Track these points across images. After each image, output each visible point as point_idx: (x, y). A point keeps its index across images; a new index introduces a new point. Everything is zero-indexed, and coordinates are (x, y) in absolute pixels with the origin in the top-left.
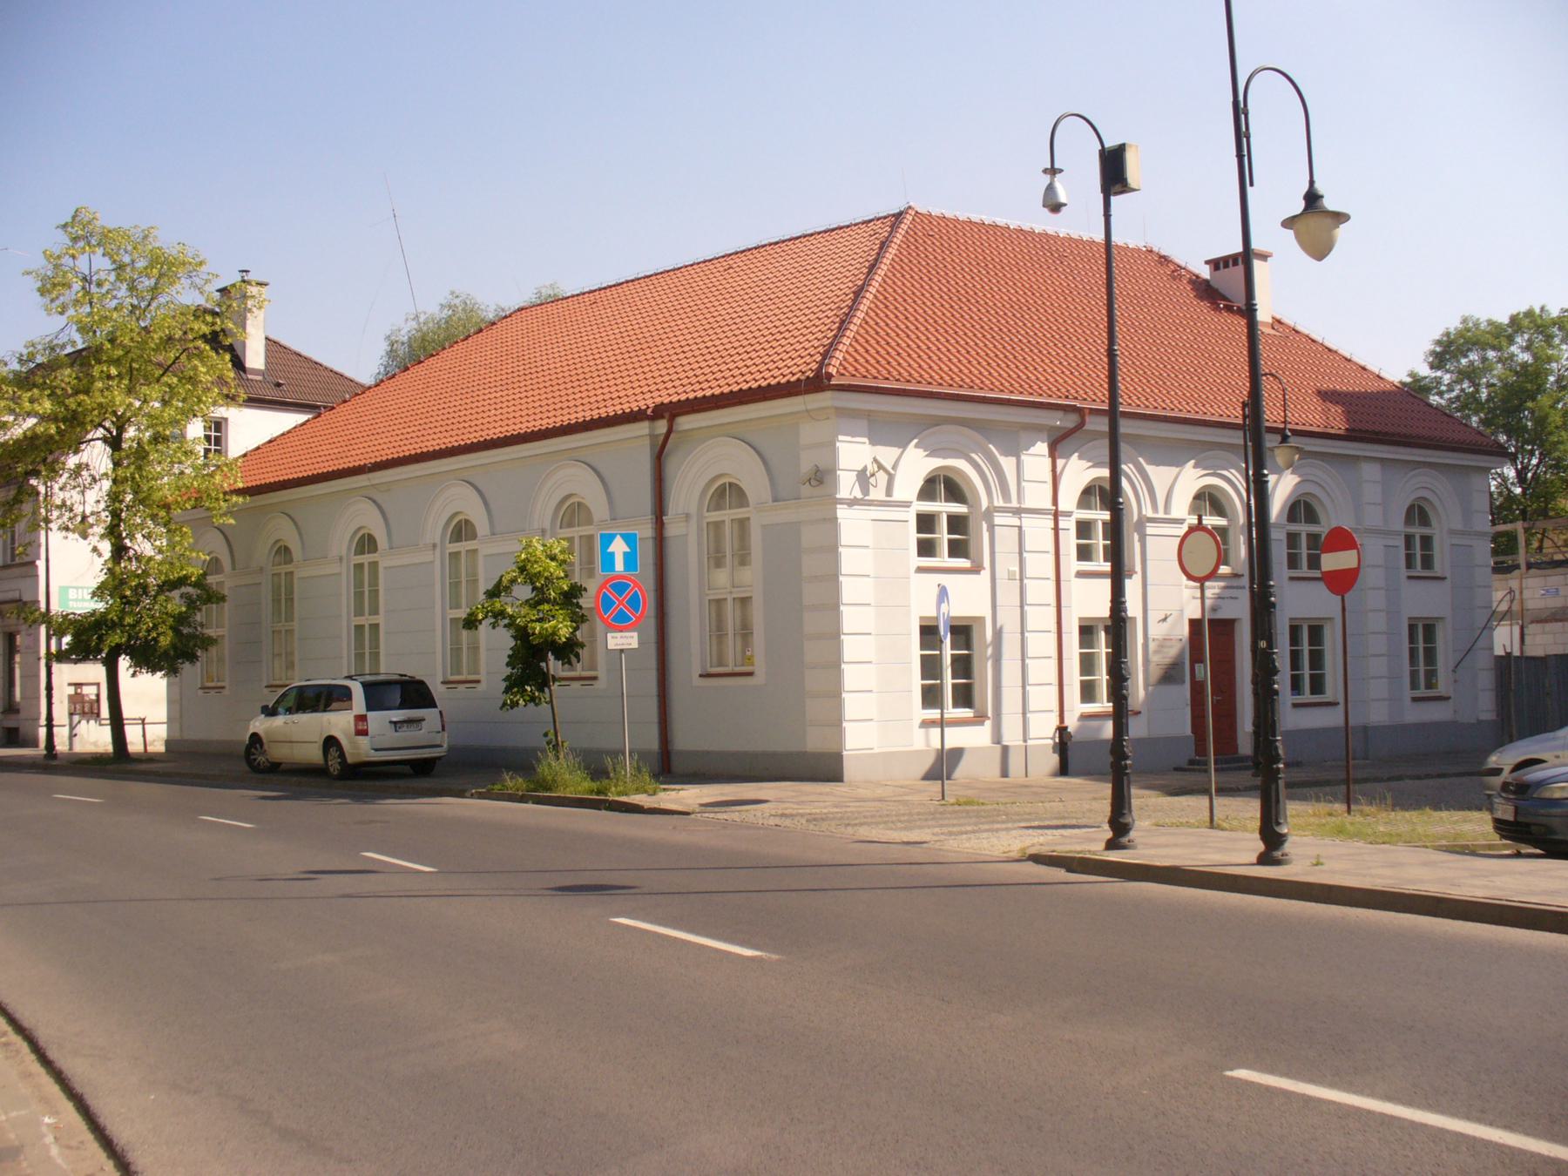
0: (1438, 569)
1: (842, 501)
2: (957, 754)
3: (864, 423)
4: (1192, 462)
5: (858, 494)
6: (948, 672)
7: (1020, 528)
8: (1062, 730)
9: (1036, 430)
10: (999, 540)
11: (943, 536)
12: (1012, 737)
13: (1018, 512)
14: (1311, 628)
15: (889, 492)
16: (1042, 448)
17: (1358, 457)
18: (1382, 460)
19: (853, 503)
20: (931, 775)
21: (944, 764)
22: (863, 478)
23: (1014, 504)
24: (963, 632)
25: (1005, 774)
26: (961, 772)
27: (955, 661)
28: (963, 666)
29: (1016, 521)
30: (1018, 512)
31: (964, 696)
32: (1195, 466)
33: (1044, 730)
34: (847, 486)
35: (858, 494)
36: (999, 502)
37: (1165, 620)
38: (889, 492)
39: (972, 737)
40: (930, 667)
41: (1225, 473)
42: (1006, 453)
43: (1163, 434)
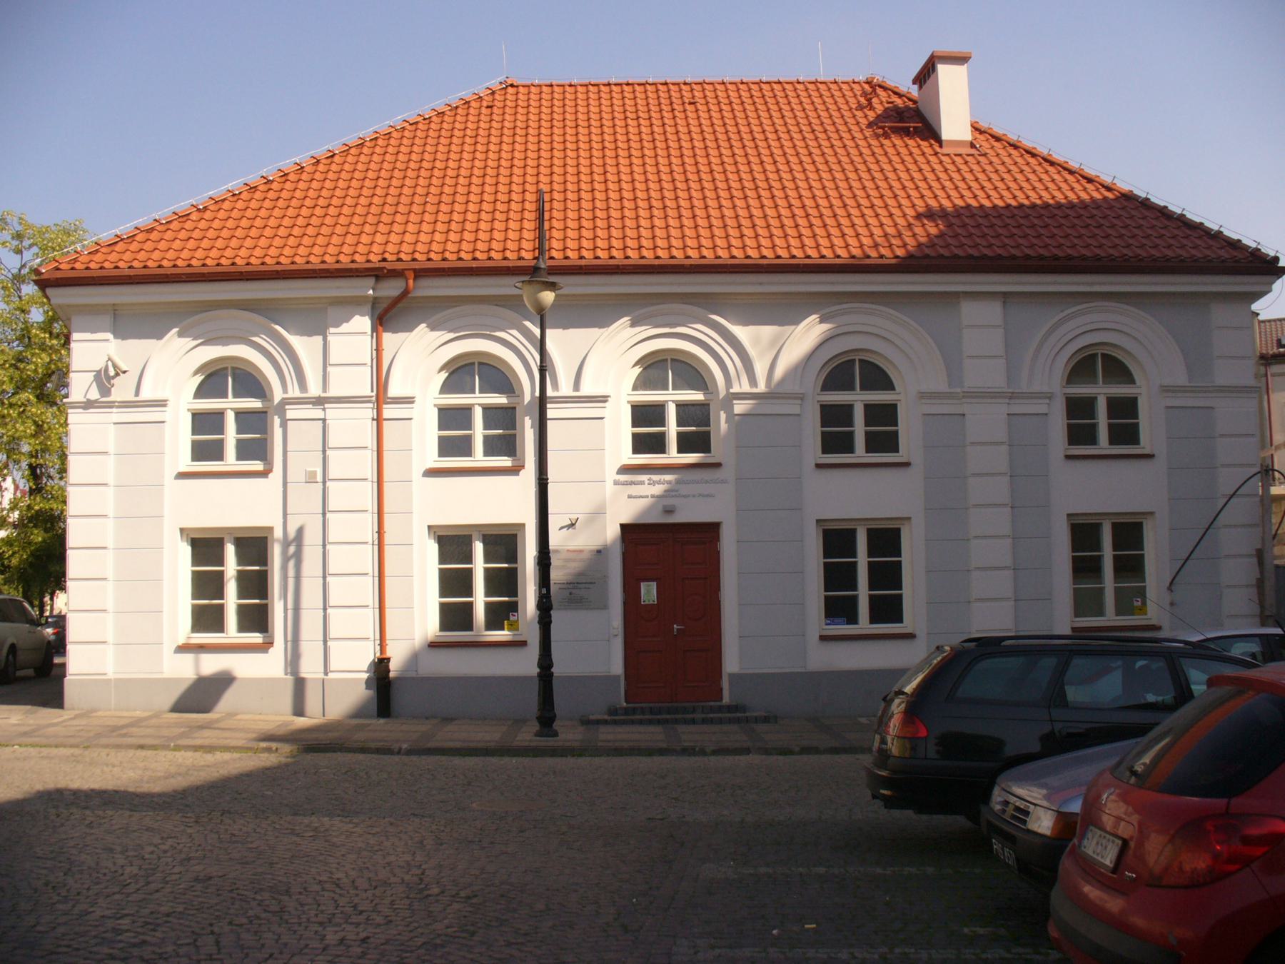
0: (1147, 441)
1: (75, 405)
2: (223, 681)
3: (108, 319)
4: (175, 330)
5: (94, 394)
6: (231, 588)
7: (324, 420)
8: (381, 665)
9: (350, 305)
10: (295, 438)
11: (231, 435)
12: (310, 668)
13: (319, 402)
14: (874, 535)
15: (577, 385)
16: (362, 323)
17: (957, 295)
18: (1005, 295)
19: (89, 405)
20: (181, 706)
21: (202, 695)
22: (104, 380)
23: (314, 390)
24: (254, 546)
25: (299, 710)
26: (228, 701)
27: (239, 577)
28: (255, 585)
29: (318, 413)
30: (319, 402)
31: (256, 619)
32: (180, 335)
33: (353, 663)
34: (80, 386)
35: (94, 394)
36: (294, 392)
37: (572, 525)
38: (577, 385)
39: (260, 668)
40: (207, 585)
41: (740, 332)
42: (308, 332)
43: (164, 299)
